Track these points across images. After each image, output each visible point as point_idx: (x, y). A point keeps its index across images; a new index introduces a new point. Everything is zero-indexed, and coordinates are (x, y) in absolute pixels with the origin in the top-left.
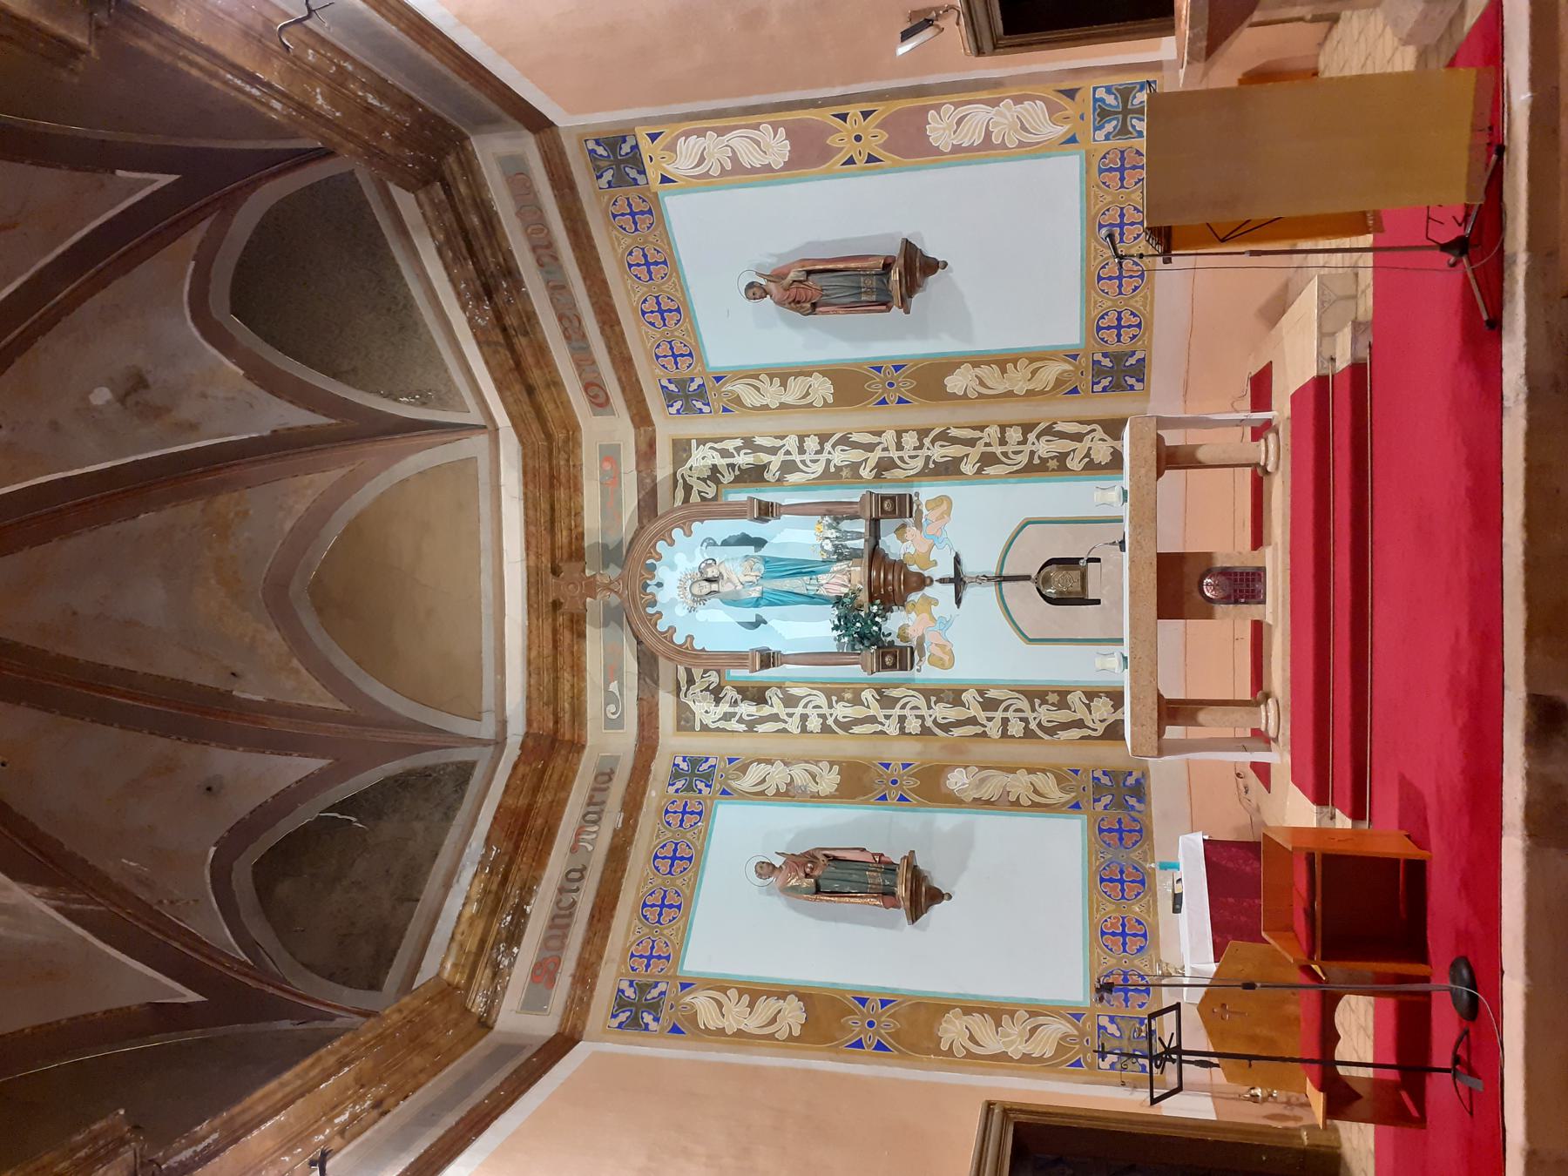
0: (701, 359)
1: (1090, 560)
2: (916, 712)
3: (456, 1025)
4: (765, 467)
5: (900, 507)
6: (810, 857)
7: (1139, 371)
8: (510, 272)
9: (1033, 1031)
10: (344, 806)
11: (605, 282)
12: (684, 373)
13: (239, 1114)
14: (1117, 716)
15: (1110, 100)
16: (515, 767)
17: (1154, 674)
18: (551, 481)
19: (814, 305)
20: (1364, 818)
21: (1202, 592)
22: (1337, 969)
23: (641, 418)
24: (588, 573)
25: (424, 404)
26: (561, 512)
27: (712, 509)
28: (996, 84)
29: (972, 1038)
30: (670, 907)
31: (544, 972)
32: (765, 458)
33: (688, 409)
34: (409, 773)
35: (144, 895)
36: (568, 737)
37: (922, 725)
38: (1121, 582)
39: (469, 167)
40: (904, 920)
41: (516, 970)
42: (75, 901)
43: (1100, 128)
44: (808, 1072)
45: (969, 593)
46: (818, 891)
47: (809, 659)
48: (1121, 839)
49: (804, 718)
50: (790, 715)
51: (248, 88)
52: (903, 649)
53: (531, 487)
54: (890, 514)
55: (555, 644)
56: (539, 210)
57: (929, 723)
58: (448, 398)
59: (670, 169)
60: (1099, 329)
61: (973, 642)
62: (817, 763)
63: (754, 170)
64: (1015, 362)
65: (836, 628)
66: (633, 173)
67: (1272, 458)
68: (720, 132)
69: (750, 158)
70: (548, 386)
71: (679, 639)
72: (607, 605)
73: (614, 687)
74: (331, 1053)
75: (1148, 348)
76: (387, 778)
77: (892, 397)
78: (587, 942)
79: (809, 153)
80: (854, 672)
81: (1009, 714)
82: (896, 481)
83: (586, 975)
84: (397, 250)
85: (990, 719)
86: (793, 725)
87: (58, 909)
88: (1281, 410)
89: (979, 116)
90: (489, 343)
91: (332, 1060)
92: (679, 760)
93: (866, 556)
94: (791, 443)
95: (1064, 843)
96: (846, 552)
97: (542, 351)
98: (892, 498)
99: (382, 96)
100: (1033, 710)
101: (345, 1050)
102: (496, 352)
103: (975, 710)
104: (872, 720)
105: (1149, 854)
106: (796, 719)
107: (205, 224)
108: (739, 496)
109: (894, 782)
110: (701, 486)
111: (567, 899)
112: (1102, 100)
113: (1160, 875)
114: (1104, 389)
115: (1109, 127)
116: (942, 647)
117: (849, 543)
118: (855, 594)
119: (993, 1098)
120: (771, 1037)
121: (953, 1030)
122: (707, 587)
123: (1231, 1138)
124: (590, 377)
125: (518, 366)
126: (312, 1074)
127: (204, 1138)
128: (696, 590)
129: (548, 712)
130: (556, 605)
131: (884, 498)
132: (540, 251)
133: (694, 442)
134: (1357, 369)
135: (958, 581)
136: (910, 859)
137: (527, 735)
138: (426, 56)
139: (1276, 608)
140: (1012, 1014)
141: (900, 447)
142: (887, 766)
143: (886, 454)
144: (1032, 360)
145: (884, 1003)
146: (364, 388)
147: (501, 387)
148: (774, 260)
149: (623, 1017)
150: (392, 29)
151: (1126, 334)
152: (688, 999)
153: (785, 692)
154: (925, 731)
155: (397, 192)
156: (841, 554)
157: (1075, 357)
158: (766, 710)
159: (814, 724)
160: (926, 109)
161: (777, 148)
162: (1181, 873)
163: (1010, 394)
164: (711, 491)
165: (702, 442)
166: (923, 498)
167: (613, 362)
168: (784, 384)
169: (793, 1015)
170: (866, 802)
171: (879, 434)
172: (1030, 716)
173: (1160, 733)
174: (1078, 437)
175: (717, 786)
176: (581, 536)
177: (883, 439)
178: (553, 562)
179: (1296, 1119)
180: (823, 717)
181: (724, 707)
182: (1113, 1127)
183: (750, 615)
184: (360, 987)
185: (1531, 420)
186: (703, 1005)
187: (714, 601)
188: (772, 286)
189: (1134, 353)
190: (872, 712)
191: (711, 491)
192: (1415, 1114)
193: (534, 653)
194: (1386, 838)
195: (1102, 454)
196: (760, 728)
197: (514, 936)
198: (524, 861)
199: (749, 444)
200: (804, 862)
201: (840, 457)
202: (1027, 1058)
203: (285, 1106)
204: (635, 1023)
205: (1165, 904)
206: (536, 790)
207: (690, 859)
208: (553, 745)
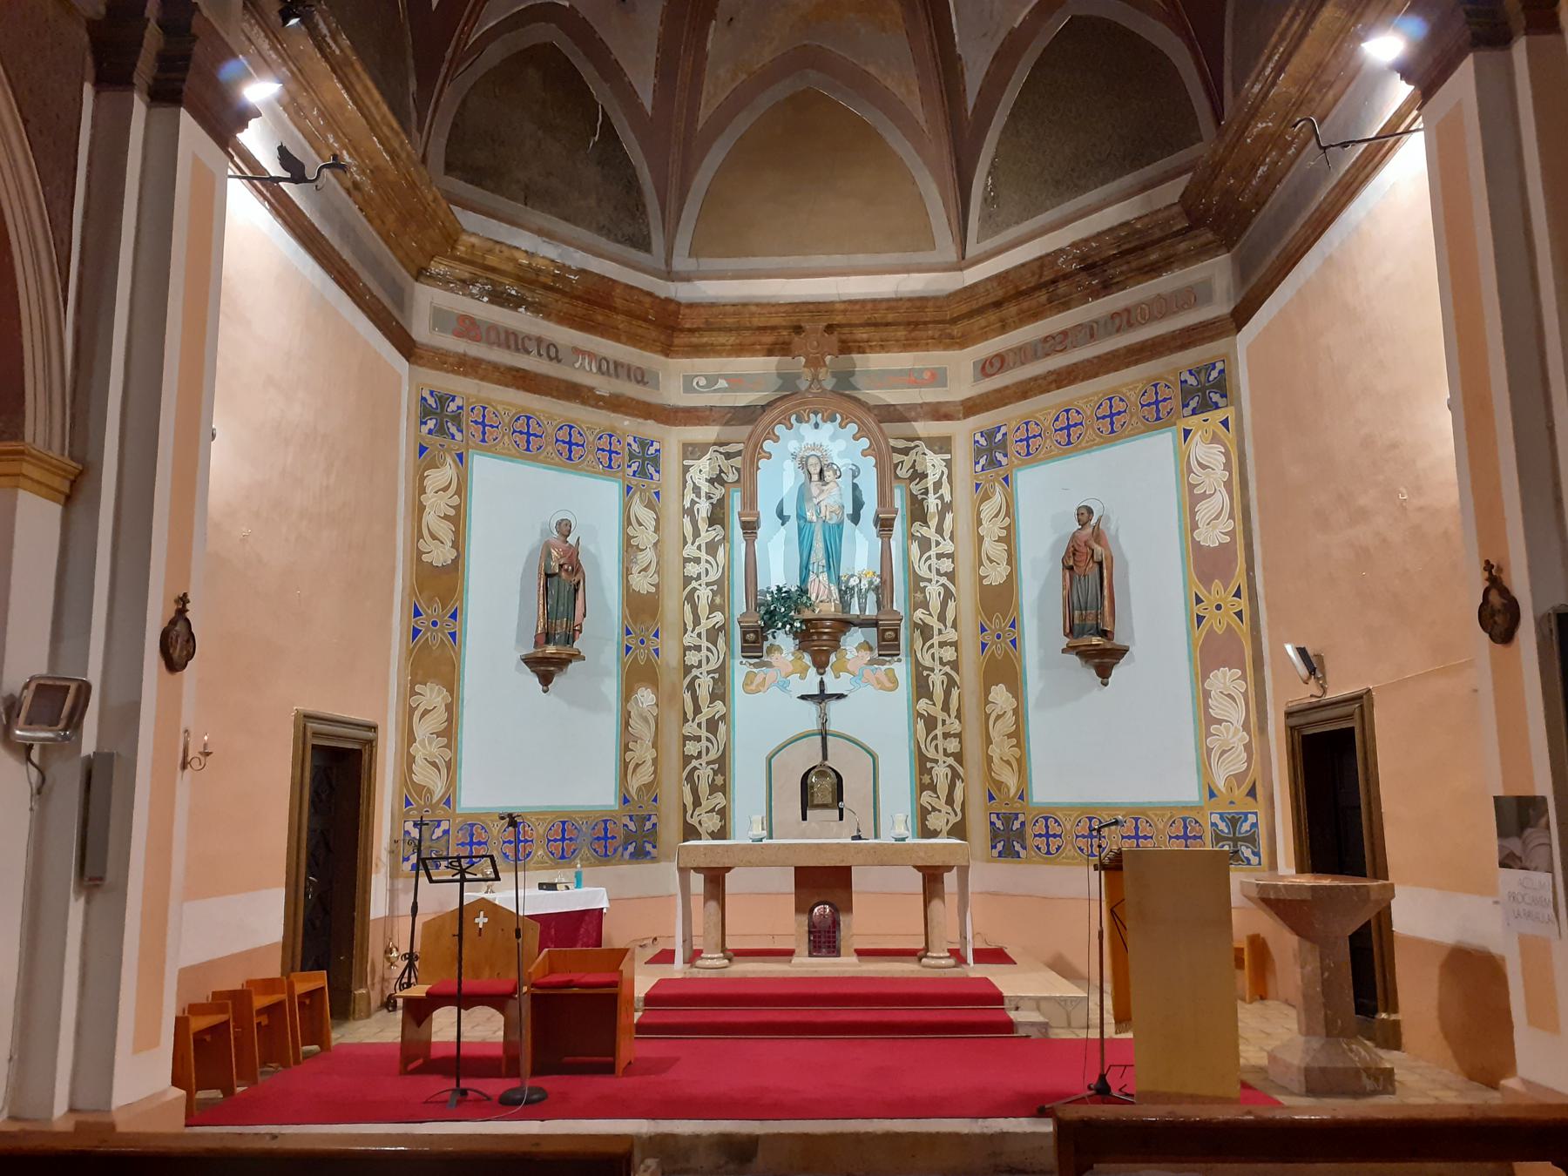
0: (1024, 464)
1: (841, 811)
2: (706, 660)
4: (925, 522)
5: (888, 645)
6: (577, 569)
7: (1009, 853)
8: (1107, 288)
9: (434, 764)
10: (608, 126)
12: (1012, 448)
13: (354, 70)
15: (1246, 827)
16: (650, 294)
17: (750, 864)
18: (914, 323)
19: (1071, 568)
22: (523, 1007)
23: (971, 408)
24: (828, 358)
25: (985, 200)
28: (1263, 729)
29: (426, 712)
30: (527, 441)
31: (468, 327)
32: (933, 523)
33: (979, 452)
34: (639, 192)
36: (676, 341)
38: (824, 837)
39: (1204, 252)
41: (468, 300)
43: (1222, 818)
45: (811, 708)
46: (548, 576)
48: (598, 839)
49: (697, 561)
50: (699, 548)
51: (1271, 65)
53: (909, 304)
55: (763, 329)
56: (1163, 316)
57: (695, 672)
58: (991, 224)
59: (1196, 438)
60: (1046, 819)
61: (768, 710)
62: (657, 572)
63: (1193, 514)
64: (1018, 745)
65: (779, 589)
66: (1193, 404)
67: (933, 962)
68: (1228, 485)
69: (1205, 511)
72: (798, 376)
73: (722, 383)
74: (402, 143)
75: (1029, 860)
76: (634, 169)
77: (988, 638)
78: (496, 367)
79: (1207, 565)
80: (739, 605)
81: (704, 743)
82: (911, 642)
84: (1128, 180)
85: (699, 725)
86: (690, 550)
88: (974, 970)
89: (1234, 714)
90: (1042, 267)
93: (845, 616)
94: (947, 547)
95: (594, 789)
96: (847, 597)
98: (897, 638)
99: (1266, 178)
101: (404, 155)
102: (1033, 274)
103: (706, 713)
104: (697, 622)
105: (588, 863)
106: (696, 554)
108: (899, 500)
109: (642, 642)
110: (907, 465)
112: (1246, 819)
113: (571, 873)
114: (992, 824)
115: (1222, 826)
116: (763, 683)
118: (811, 606)
120: (421, 536)
121: (432, 695)
122: (815, 471)
124: (1010, 359)
125: (1019, 294)
126: (385, 129)
127: (335, 41)
128: (812, 461)
129: (699, 323)
130: (798, 329)
131: (897, 632)
133: (948, 456)
134: (1009, 1026)
135: (822, 697)
136: (577, 656)
137: (679, 304)
138: (1300, 222)
139: (806, 966)
140: (448, 746)
141: (942, 645)
142: (656, 635)
143: (936, 632)
144: (1019, 761)
145: (453, 635)
147: (1002, 278)
150: (1321, 195)
151: (1041, 842)
152: (449, 460)
154: (687, 669)
155: (1185, 180)
156: (845, 593)
157: (1021, 797)
158: (703, 526)
159: (692, 570)
161: (1212, 535)
162: (573, 890)
163: (988, 741)
165: (948, 464)
166: (895, 666)
167: (1021, 383)
168: (1000, 540)
169: (440, 555)
170: (624, 617)
171: (954, 626)
172: (704, 760)
173: (697, 870)
174: (950, 801)
175: (634, 481)
176: (861, 351)
178: (838, 325)
180: (699, 577)
181: (705, 488)
183: (790, 510)
184: (447, 155)
187: (803, 477)
189: (1024, 848)
191: (903, 472)
192: (411, 1067)
193: (753, 309)
194: (629, 1048)
195: (934, 822)
196: (687, 520)
197: (498, 298)
198: (563, 305)
199: (946, 507)
201: (933, 591)
202: (411, 760)
203: (360, 109)
204: (426, 413)
205: (546, 877)
206: (630, 314)
207: (570, 458)
208: (669, 327)
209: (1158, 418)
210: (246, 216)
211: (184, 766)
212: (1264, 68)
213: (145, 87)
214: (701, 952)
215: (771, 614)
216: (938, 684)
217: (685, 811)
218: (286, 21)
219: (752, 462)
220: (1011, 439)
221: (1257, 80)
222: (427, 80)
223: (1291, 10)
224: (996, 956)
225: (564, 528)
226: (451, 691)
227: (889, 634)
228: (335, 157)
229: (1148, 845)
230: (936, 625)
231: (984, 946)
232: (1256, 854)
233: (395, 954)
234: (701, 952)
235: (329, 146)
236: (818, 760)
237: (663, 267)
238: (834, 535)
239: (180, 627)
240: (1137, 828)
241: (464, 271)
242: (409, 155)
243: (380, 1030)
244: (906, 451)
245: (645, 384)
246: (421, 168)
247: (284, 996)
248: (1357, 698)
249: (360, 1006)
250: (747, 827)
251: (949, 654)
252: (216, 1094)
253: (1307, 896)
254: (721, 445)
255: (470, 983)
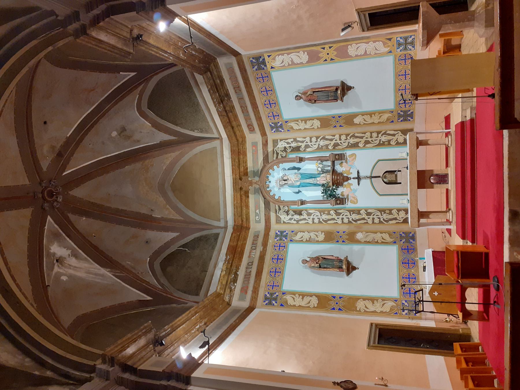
2: (347, 216)
3: (222, 304)
4: (300, 147)
6: (317, 258)
7: (412, 115)
8: (228, 95)
9: (383, 305)
10: (184, 246)
11: (254, 96)
12: (276, 120)
14: (406, 216)
15: (401, 41)
16: (232, 234)
17: (417, 204)
19: (315, 101)
20: (474, 242)
21: (430, 181)
22: (466, 281)
23: (264, 134)
25: (201, 132)
26: (241, 162)
27: (285, 160)
28: (368, 38)
29: (366, 307)
30: (278, 272)
31: (244, 290)
32: (300, 144)
33: (277, 131)
34: (201, 237)
35: (134, 271)
36: (245, 225)
37: (349, 221)
38: (407, 178)
39: (217, 66)
40: (345, 275)
41: (236, 290)
42: (117, 273)
44: (320, 316)
45: (362, 182)
46: (320, 267)
47: (317, 202)
48: (408, 251)
49: (313, 219)
50: (309, 218)
52: (342, 199)
54: (338, 159)
56: (236, 77)
57: (351, 220)
58: (208, 130)
59: (273, 65)
60: (399, 104)
61: (363, 196)
62: (317, 232)
63: (298, 64)
66: (263, 66)
67: (450, 143)
68: (288, 54)
69: (296, 60)
70: (237, 126)
71: (276, 197)
72: (255, 188)
73: (257, 211)
74: (193, 310)
75: (414, 109)
78: (255, 282)
79: (314, 58)
80: (328, 206)
81: (375, 217)
83: (256, 291)
85: (369, 218)
86: (310, 221)
87: (114, 275)
88: (453, 129)
89: (363, 47)
90: (222, 115)
91: (193, 312)
92: (277, 232)
94: (308, 139)
95: (392, 253)
97: (236, 116)
98: (338, 155)
100: (382, 215)
101: (196, 309)
102: (224, 118)
104: (334, 219)
105: (416, 255)
106: (311, 219)
107: (143, 85)
108: (293, 156)
109: (341, 237)
110: (282, 153)
111: (249, 270)
113: (419, 261)
114: (401, 121)
115: (401, 48)
117: (326, 168)
118: (328, 183)
119: (372, 322)
120: (309, 307)
121: (360, 305)
122: (284, 182)
123: (439, 331)
124: (249, 123)
125: (230, 122)
127: (166, 330)
128: (281, 183)
130: (241, 189)
131: (336, 155)
132: (236, 89)
134: (472, 120)
135: (359, 178)
136: (346, 258)
139: (452, 184)
140: (377, 300)
141: (340, 139)
142: (338, 232)
145: (340, 298)
146: (185, 128)
147: (225, 127)
148: (303, 88)
149: (267, 302)
152: (285, 297)
153: (307, 212)
154: (350, 222)
156: (323, 172)
157: (392, 112)
158: (302, 217)
159: (316, 221)
160: (348, 45)
161: (304, 57)
162: (426, 260)
163: (373, 123)
164: (284, 154)
165: (281, 140)
166: (348, 154)
167: (256, 119)
168: (306, 123)
169: (314, 301)
170: (333, 243)
171: (334, 136)
172: (381, 217)
173: (419, 221)
174: (394, 135)
175: (289, 239)
177: (335, 137)
179: (458, 327)
180: (319, 218)
181: (290, 216)
182: (406, 329)
183: (297, 190)
184: (194, 295)
185: (509, 141)
186: (289, 298)
187: (286, 186)
188: (303, 96)
190: (333, 217)
191: (284, 154)
192: (486, 318)
193: (235, 202)
194: (480, 247)
195: (401, 140)
196: (300, 222)
197: (235, 280)
198: (236, 261)
199: (295, 140)
200: (316, 259)
201: (322, 143)
202: (382, 312)
203: (185, 323)
204: (270, 303)
206: (238, 241)
208: (241, 228)
209: (268, 77)
210: (219, 357)
211: (386, 386)
212: (166, 57)
213: (186, 386)
214: (447, 220)
215: (330, 196)
216: (353, 140)
217: (398, 223)
218: (164, 345)
219: (282, 202)
220: (273, 121)
221: (169, 58)
222: (171, 301)
223: (150, 51)
224: (447, 119)
225: (305, 262)
226: (359, 299)
227: (337, 157)
228: (202, 332)
229: (408, 87)
230: (334, 141)
231: (444, 122)
232: (411, 37)
233: (448, 319)
234: (447, 220)
235: (195, 332)
236: (380, 179)
237: (223, 229)
238: (305, 176)
239: (343, 384)
240: (402, 75)
241: (228, 291)
242: (196, 308)
243: (474, 327)
244: (277, 154)
245: (258, 235)
246: (200, 304)
247: (462, 358)
248: (358, 13)
249: (466, 331)
250: (403, 202)
251: (343, 137)
252: (496, 381)
253: (426, 31)
254: (276, 211)
255: (457, 299)
